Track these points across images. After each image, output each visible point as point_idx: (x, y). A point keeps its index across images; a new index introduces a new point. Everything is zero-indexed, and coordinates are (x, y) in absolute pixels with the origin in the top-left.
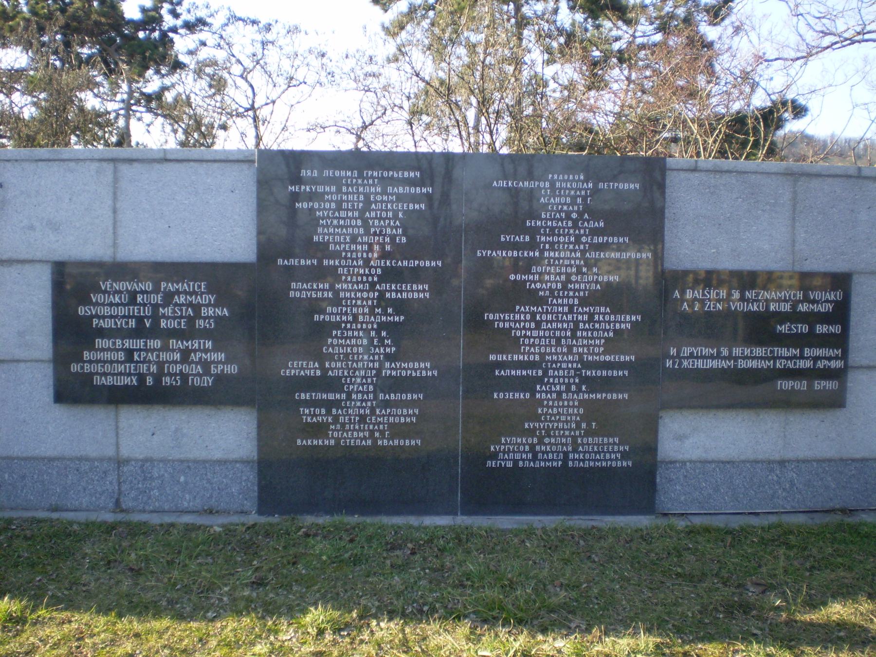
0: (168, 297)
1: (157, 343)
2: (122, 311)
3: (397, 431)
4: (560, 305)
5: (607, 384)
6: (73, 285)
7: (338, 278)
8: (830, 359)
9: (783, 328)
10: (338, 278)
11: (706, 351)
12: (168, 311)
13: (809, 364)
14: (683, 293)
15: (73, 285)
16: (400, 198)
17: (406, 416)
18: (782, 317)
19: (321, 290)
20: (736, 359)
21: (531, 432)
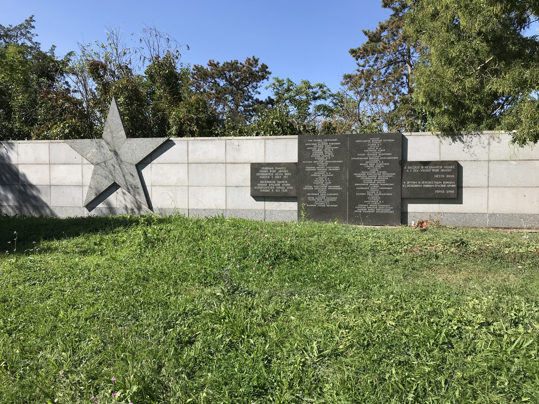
0: (277, 171)
1: (274, 182)
3: (331, 203)
5: (385, 191)
6: (256, 168)
7: (317, 166)
8: (451, 184)
10: (317, 166)
11: (414, 183)
14: (407, 167)
15: (256, 168)
16: (332, 146)
17: (334, 199)
20: (423, 184)
21: (366, 203)
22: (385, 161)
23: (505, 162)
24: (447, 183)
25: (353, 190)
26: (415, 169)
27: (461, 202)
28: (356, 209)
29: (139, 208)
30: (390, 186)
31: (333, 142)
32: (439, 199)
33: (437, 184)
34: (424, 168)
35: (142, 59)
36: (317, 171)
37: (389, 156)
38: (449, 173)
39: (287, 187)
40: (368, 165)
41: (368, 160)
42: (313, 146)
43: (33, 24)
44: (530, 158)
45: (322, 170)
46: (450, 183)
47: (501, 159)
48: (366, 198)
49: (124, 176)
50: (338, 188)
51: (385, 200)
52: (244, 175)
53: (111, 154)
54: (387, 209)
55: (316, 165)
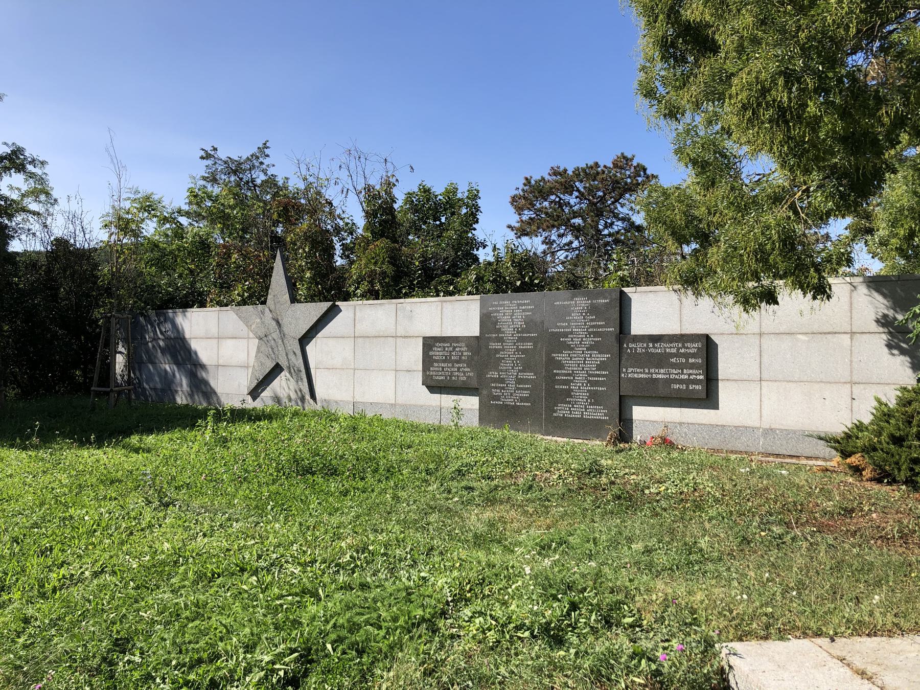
0: (454, 348)
1: (450, 365)
2: (441, 353)
3: (522, 399)
4: (579, 351)
6: (429, 343)
7: (504, 342)
8: (696, 375)
9: (673, 360)
10: (504, 342)
11: (638, 370)
12: (453, 353)
13: (686, 377)
14: (628, 345)
15: (429, 343)
16: (524, 311)
17: (526, 394)
18: (672, 355)
19: (498, 346)
20: (652, 374)
21: (569, 403)
22: (596, 334)
23: (787, 336)
24: (695, 371)
25: (551, 379)
26: (640, 347)
27: (716, 407)
28: (555, 411)
29: (303, 399)
30: (603, 376)
31: (524, 304)
32: (689, 400)
33: (674, 373)
34: (654, 347)
35: (345, 192)
36: (503, 350)
37: (599, 327)
38: (693, 356)
39: (464, 374)
40: (572, 341)
41: (571, 333)
42: (498, 311)
43: (267, 151)
44: (830, 330)
45: (510, 348)
46: (695, 372)
47: (782, 330)
48: (568, 393)
49: (287, 355)
50: (530, 376)
51: (595, 398)
52: (414, 354)
53: (274, 323)
54: (599, 413)
55: (501, 340)
